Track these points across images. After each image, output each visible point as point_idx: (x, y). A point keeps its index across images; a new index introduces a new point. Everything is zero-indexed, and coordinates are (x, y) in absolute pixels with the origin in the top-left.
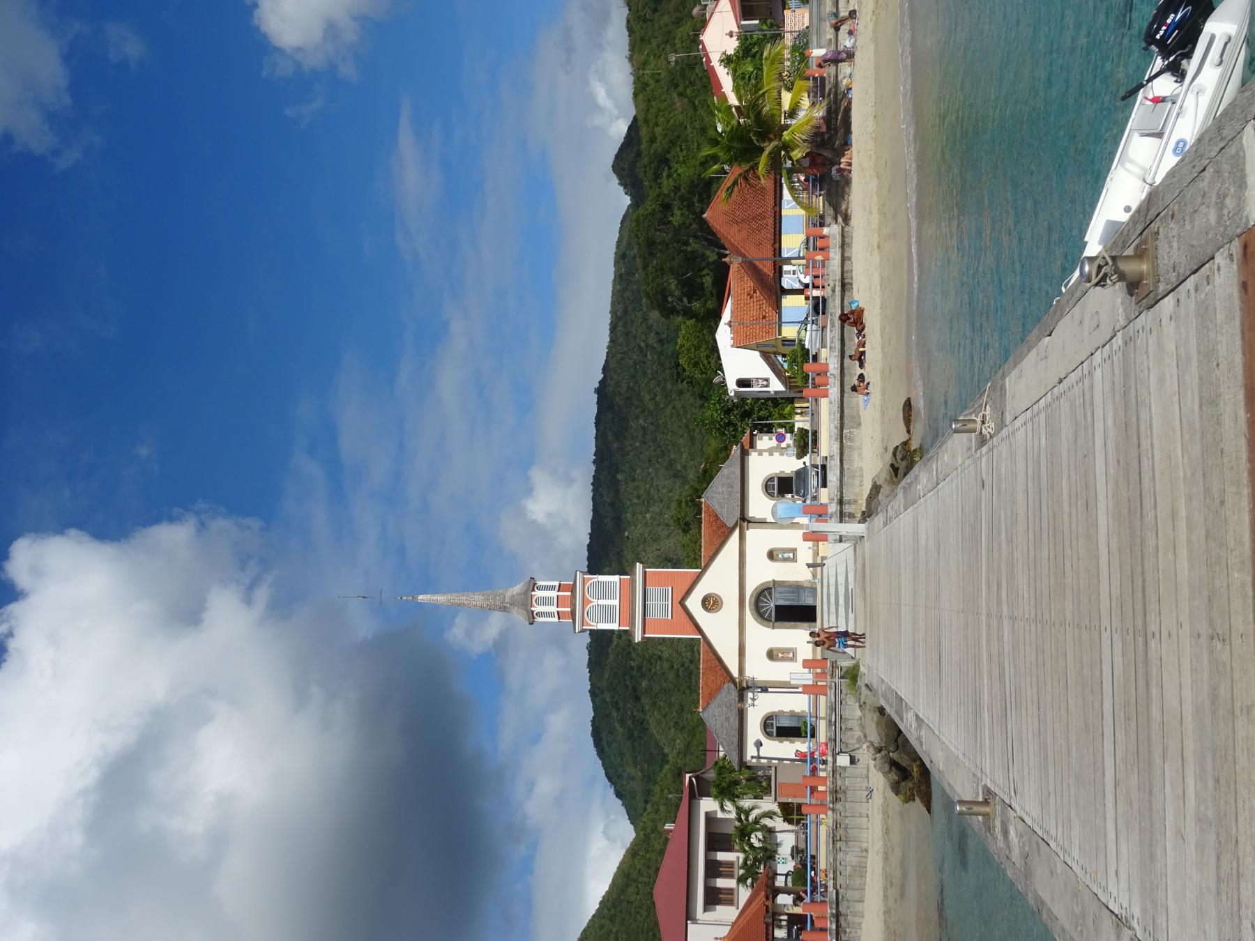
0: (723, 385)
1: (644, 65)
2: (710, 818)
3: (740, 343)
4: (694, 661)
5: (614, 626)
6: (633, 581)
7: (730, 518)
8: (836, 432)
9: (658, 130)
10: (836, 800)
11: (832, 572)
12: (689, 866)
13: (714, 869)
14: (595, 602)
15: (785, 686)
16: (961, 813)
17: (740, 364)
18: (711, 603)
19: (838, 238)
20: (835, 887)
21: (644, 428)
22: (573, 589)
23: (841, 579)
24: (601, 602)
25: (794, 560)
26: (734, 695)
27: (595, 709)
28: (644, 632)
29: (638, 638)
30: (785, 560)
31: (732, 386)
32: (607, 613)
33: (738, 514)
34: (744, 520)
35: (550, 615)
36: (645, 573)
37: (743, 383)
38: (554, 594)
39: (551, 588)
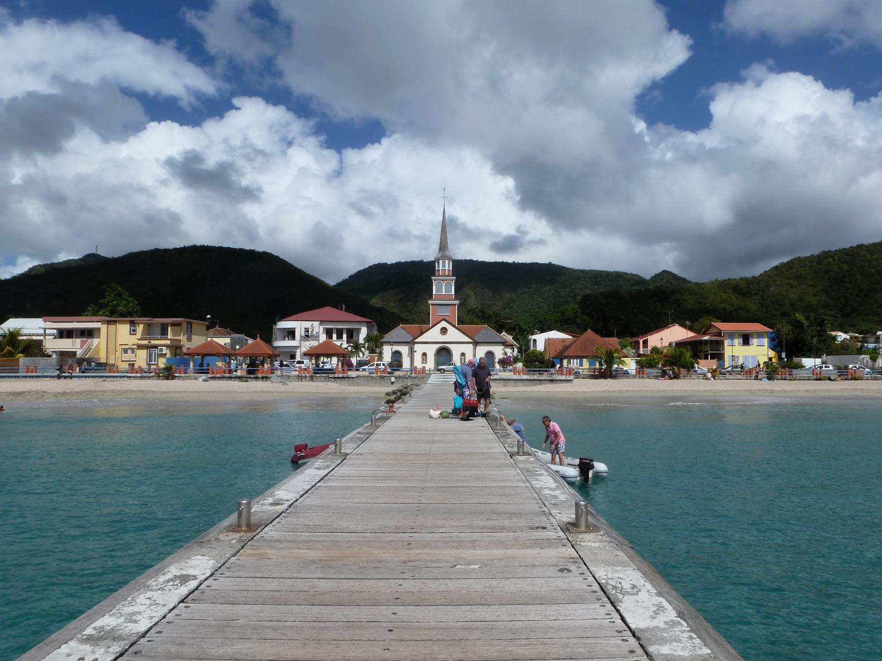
2: (359, 330)
3: (548, 342)
4: (424, 323)
16: (240, 504)
17: (540, 341)
18: (444, 331)
29: (430, 302)
32: (439, 289)
34: (476, 343)
37: (535, 341)
38: (447, 268)
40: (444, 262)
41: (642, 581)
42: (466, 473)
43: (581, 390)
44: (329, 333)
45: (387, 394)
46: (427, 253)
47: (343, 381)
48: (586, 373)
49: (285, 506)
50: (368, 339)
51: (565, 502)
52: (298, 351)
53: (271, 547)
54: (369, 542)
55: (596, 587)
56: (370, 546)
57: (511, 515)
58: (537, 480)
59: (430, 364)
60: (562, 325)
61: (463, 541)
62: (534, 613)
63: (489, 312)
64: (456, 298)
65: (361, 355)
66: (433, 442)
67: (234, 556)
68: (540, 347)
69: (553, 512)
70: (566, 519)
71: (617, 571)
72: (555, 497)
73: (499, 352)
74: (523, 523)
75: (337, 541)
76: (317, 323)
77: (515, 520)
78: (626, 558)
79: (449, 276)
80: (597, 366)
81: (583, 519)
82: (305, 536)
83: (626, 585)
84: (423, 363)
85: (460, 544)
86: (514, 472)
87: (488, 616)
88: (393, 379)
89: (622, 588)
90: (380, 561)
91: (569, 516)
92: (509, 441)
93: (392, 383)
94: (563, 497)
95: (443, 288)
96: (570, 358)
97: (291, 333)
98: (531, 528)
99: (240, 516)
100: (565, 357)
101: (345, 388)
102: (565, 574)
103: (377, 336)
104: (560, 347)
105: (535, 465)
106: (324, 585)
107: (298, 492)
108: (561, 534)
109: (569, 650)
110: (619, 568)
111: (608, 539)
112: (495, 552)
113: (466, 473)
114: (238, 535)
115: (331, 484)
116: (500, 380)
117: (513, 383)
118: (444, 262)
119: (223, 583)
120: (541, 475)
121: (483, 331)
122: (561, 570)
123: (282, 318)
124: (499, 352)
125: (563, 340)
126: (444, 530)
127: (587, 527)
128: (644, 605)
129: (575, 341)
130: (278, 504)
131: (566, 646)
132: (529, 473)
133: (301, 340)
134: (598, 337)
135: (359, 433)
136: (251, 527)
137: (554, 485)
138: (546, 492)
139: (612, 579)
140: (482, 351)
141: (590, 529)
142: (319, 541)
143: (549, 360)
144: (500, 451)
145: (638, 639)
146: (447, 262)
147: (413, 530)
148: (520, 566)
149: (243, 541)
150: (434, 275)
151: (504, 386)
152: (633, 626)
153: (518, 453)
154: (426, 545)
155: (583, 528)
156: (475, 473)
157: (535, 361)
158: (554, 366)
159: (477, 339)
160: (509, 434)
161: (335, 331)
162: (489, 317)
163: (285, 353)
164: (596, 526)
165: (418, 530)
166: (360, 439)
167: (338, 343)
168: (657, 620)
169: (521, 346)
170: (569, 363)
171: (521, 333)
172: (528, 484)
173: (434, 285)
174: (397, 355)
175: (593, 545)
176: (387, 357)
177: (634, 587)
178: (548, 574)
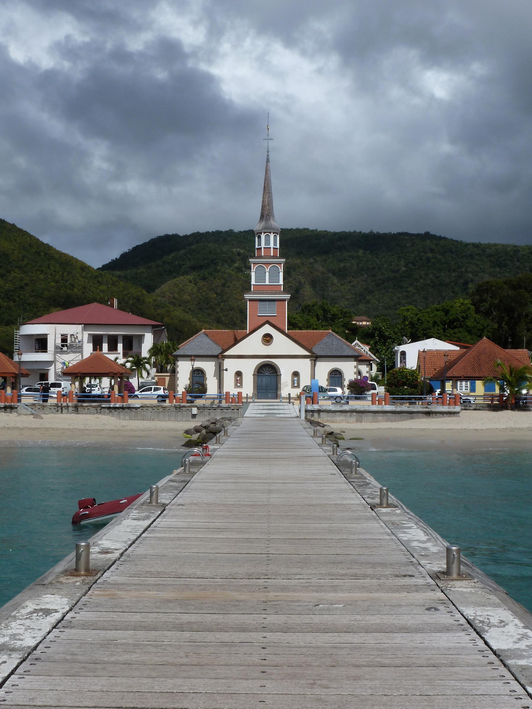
2: (141, 338)
3: (423, 355)
5: (253, 282)
6: (280, 294)
11: (285, 407)
14: (267, 270)
17: (411, 354)
18: (268, 339)
21: (398, 271)
23: (281, 412)
24: (267, 274)
25: (293, 387)
27: (186, 237)
28: (250, 300)
29: (247, 296)
30: (293, 382)
31: (402, 348)
32: (261, 277)
34: (315, 358)
35: (260, 244)
36: (284, 300)
37: (403, 354)
38: (272, 245)
39: (275, 244)
40: (268, 237)
41: (511, 618)
42: (317, 525)
43: (472, 427)
44: (97, 341)
45: (187, 432)
46: (239, 212)
47: (122, 413)
48: (480, 401)
49: (117, 554)
50: (155, 351)
51: (436, 553)
52: (52, 368)
53: (118, 589)
54: (221, 585)
55: (463, 621)
56: (224, 589)
57: (374, 565)
58: (405, 533)
59: (248, 388)
60: (444, 330)
61: (323, 586)
62: (399, 639)
63: (335, 310)
64: (285, 291)
65: (145, 374)
66: (270, 492)
67: (84, 595)
68: (412, 363)
69: (422, 562)
70: (436, 568)
71: (488, 610)
72: (425, 549)
73: (349, 370)
74: (388, 571)
75: (187, 585)
76: (80, 327)
77: (379, 569)
78: (497, 601)
79: (274, 257)
80: (497, 391)
81: (455, 566)
82: (152, 580)
83: (494, 620)
84: (236, 386)
85: (320, 589)
86: (377, 525)
87: (355, 640)
88: (195, 411)
89: (490, 622)
90: (237, 601)
91: (441, 565)
92: (369, 491)
93: (194, 416)
94: (434, 549)
95: (267, 276)
96: (455, 379)
97: (41, 343)
98: (397, 576)
99: (78, 557)
100: (449, 379)
101: (124, 423)
102: (433, 611)
103: (168, 347)
104: (440, 364)
105: (403, 518)
106: (186, 618)
107: (125, 542)
108: (430, 580)
109: (432, 661)
110: (490, 608)
111: (482, 586)
112: (359, 595)
113: (317, 525)
114: (79, 579)
115: (158, 535)
116: (352, 411)
117: (370, 417)
118: (268, 237)
119: (83, 616)
120: (410, 528)
121: (326, 340)
122: (429, 609)
123: (31, 319)
124: (349, 370)
125: (446, 354)
126: (301, 577)
127: (459, 574)
128: (509, 634)
129: (460, 357)
130: (107, 553)
131: (430, 659)
132: (395, 527)
133: (56, 353)
134: (497, 349)
135: (171, 481)
136: (89, 572)
137: (425, 538)
138: (415, 544)
139: (480, 616)
140: (324, 368)
141: (461, 576)
142: (169, 585)
143: (424, 382)
144: (358, 502)
145: (498, 656)
146: (272, 236)
147: (267, 577)
148: (385, 606)
149: (88, 583)
150: (254, 257)
151: (358, 421)
152: (495, 648)
153: (381, 505)
154: (284, 589)
155: (455, 576)
156: (328, 525)
157: (404, 384)
158: (431, 391)
159: (317, 351)
160: (368, 484)
161: (105, 339)
162: (334, 317)
163: (33, 370)
164: (469, 575)
165: (273, 577)
166: (176, 488)
167: (112, 357)
168: (520, 644)
169: (383, 361)
170: (454, 386)
171: (382, 341)
172: (394, 537)
173: (253, 269)
174: (198, 375)
175: (465, 590)
176: (183, 379)
177: (502, 621)
178: (415, 612)
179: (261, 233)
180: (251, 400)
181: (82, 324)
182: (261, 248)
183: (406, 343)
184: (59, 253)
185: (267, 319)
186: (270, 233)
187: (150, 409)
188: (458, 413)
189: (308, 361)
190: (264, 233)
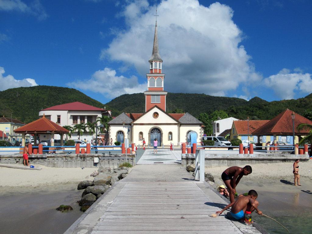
0: (217, 119)
1: (283, 103)
7: (181, 120)
8: (226, 157)
9: (267, 107)
10: (81, 157)
11: (167, 153)
12: (83, 111)
13: (82, 118)
15: (131, 138)
18: (156, 115)
19: (303, 158)
20: (48, 157)
21: (195, 105)
22: (159, 73)
24: (156, 82)
26: (129, 122)
28: (147, 95)
31: (217, 122)
33: (182, 123)
35: (152, 67)
36: (164, 95)
37: (218, 124)
38: (158, 68)
39: (160, 67)
84: (169, 140)
87: (182, 212)
93: (95, 164)
123: (45, 109)
146: (158, 63)
159: (181, 120)
179: (153, 62)
180: (147, 147)
181: (67, 110)
182: (152, 69)
183: (219, 119)
184: (92, 99)
185: (156, 104)
186: (157, 61)
187: (60, 159)
188: (308, 160)
189: (176, 127)
190: (154, 61)
